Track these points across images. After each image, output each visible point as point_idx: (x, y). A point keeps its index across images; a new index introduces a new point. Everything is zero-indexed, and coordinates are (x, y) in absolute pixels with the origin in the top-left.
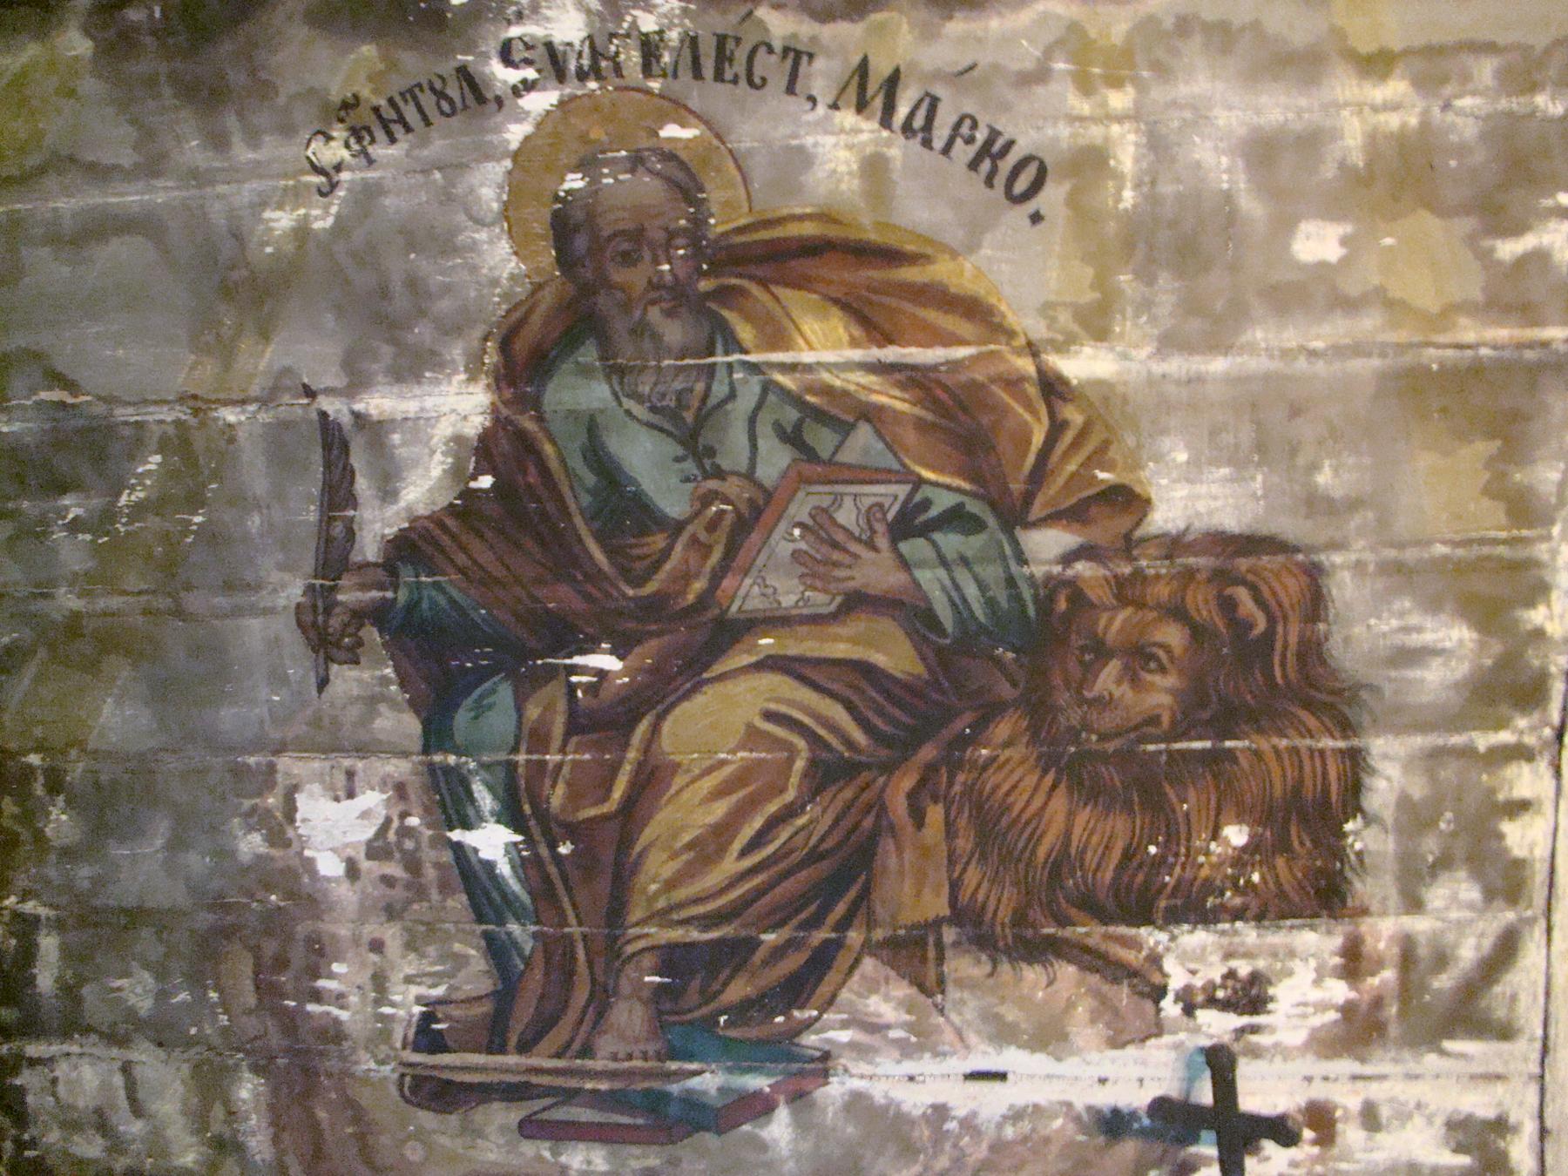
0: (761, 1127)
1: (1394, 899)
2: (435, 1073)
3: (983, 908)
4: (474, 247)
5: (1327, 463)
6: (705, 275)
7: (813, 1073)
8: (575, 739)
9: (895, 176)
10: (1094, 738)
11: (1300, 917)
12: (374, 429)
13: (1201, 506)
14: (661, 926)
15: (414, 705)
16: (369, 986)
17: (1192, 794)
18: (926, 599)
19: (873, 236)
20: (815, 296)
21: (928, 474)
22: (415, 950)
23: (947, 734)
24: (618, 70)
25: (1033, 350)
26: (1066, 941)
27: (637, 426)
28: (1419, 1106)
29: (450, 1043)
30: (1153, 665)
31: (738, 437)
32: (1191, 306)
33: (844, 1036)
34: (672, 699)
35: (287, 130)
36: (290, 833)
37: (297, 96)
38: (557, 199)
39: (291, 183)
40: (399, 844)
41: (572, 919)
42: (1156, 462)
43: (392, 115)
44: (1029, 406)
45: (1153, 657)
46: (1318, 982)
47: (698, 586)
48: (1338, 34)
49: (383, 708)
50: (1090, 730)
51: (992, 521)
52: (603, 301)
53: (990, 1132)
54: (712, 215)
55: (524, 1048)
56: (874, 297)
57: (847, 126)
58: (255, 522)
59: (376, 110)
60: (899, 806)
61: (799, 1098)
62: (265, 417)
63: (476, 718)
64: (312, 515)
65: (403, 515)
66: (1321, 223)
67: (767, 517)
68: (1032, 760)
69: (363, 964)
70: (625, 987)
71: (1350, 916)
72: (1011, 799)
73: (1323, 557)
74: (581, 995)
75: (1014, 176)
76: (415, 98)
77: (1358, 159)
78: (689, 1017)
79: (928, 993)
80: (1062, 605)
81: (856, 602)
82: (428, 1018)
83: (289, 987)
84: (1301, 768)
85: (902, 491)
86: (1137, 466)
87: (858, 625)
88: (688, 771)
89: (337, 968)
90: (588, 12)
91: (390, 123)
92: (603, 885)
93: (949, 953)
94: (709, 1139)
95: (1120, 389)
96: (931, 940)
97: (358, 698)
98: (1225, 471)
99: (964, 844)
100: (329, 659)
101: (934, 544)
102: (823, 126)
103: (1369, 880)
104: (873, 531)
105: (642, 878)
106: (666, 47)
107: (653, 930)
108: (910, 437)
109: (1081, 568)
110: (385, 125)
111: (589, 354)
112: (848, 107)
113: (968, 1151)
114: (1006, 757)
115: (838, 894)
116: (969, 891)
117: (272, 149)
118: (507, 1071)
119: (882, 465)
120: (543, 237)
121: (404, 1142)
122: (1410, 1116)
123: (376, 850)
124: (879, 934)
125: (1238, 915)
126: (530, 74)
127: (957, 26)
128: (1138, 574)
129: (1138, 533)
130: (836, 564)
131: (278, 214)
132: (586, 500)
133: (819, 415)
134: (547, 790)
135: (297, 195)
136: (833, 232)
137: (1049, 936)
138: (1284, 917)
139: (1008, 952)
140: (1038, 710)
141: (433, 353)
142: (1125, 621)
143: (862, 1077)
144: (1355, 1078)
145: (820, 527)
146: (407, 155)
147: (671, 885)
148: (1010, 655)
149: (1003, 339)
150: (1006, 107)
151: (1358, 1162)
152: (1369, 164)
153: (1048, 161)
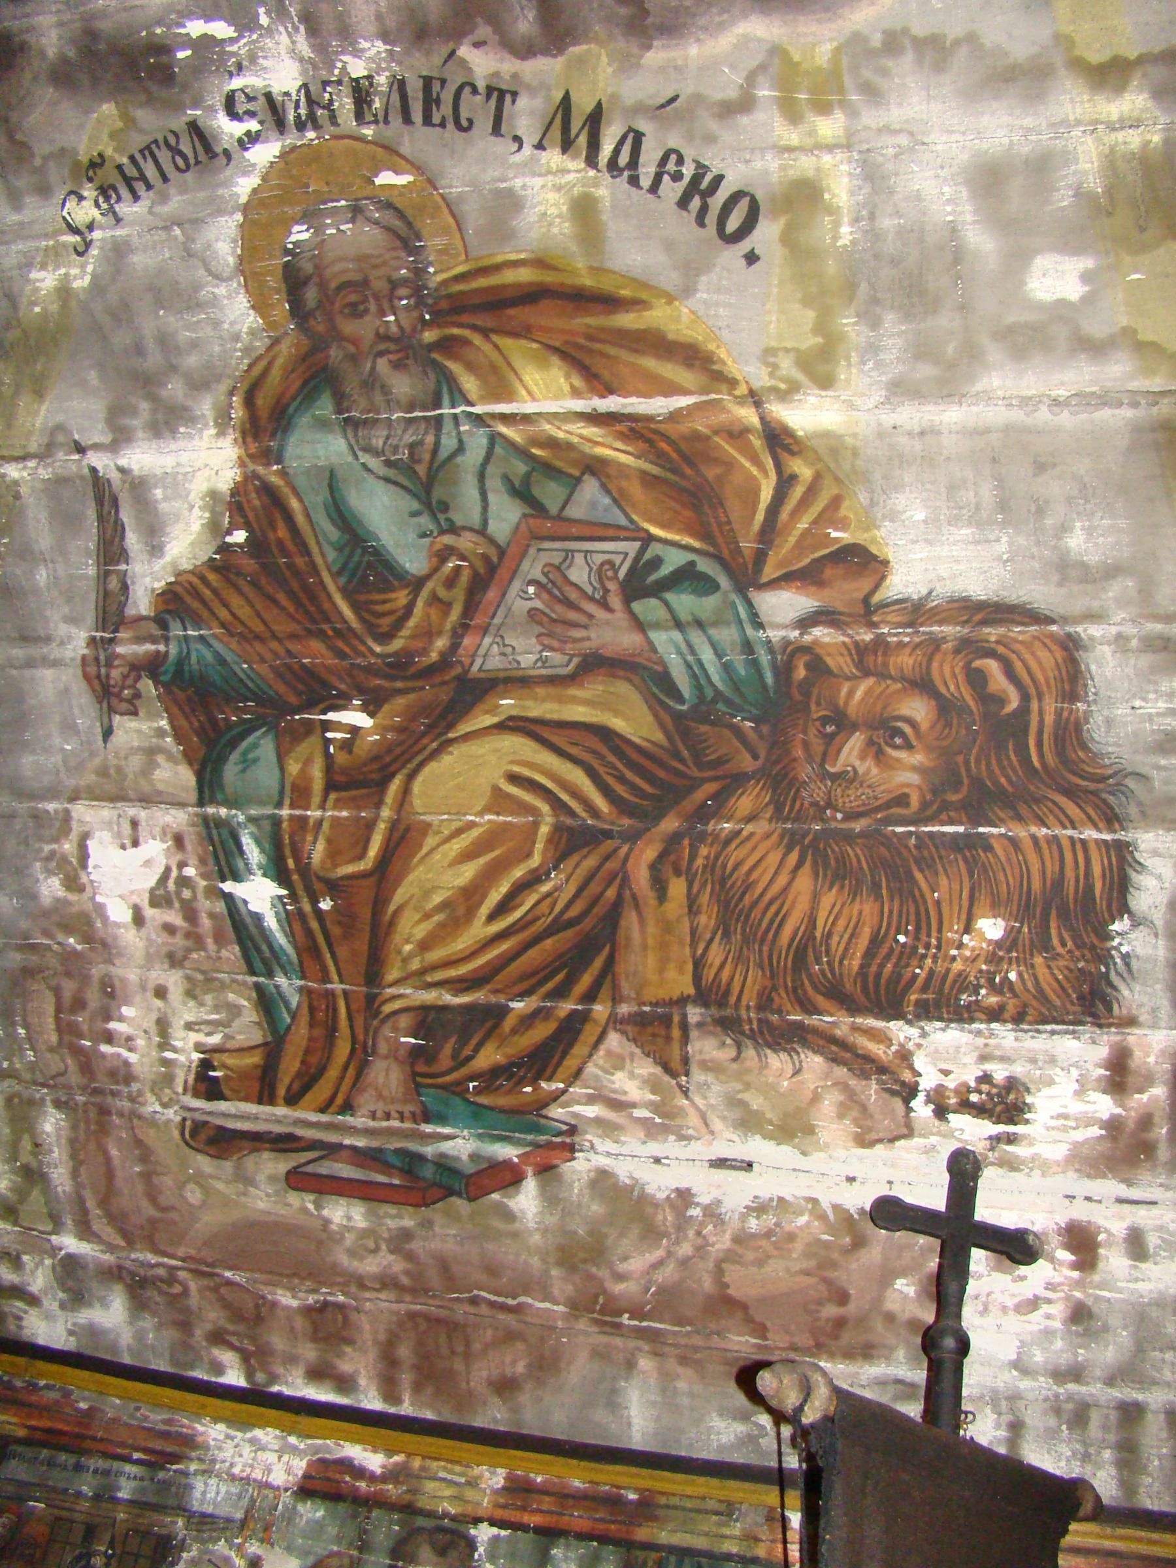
3: (727, 992)
4: (214, 301)
7: (563, 1146)
8: (333, 796)
9: (604, 218)
10: (839, 816)
11: (1064, 1023)
12: (139, 486)
13: (943, 570)
14: (416, 988)
16: (153, 1029)
17: (943, 881)
19: (588, 282)
20: (535, 346)
21: (655, 531)
22: (194, 997)
25: (755, 398)
26: (815, 1031)
27: (371, 479)
29: (227, 1092)
32: (922, 351)
33: (591, 1111)
34: (420, 758)
35: (44, 191)
36: (84, 879)
37: (51, 156)
38: (287, 252)
40: (178, 893)
41: (336, 977)
44: (755, 460)
45: (898, 732)
46: (1080, 1093)
47: (441, 643)
48: (1064, 41)
50: (836, 809)
51: (724, 581)
52: (335, 354)
53: (734, 1224)
54: (430, 264)
55: (292, 1100)
59: (119, 167)
60: (641, 877)
61: (546, 1170)
62: (45, 473)
63: (244, 771)
66: (1059, 258)
67: (503, 573)
68: (775, 837)
69: (149, 1009)
70: (383, 1048)
71: (1118, 1026)
73: (1079, 629)
74: (343, 1049)
75: (728, 216)
77: (1095, 185)
78: (440, 1080)
79: (673, 1074)
80: (801, 673)
81: (594, 664)
82: (206, 1065)
83: (85, 1028)
85: (632, 547)
87: (594, 688)
88: (438, 832)
89: (126, 1011)
90: (302, 60)
91: (134, 183)
93: (694, 1034)
95: (849, 440)
96: (676, 1019)
97: (139, 749)
100: (111, 710)
101: (667, 604)
102: (530, 168)
104: (606, 591)
105: (397, 938)
106: (377, 93)
107: (409, 991)
108: (636, 490)
109: (819, 633)
110: (128, 181)
111: (324, 407)
112: (553, 146)
115: (587, 963)
116: (713, 971)
117: (36, 211)
123: (158, 898)
124: (624, 1009)
125: (995, 1015)
126: (253, 125)
127: (656, 56)
128: (880, 641)
129: (877, 598)
131: (42, 274)
132: (331, 555)
133: (549, 470)
135: (57, 254)
136: (548, 278)
137: (795, 1022)
138: (1045, 1022)
139: (752, 1036)
140: (780, 781)
141: (186, 409)
143: (608, 1154)
144: (1121, 1201)
145: (554, 586)
146: (150, 212)
147: (424, 946)
149: (724, 387)
152: (1110, 191)
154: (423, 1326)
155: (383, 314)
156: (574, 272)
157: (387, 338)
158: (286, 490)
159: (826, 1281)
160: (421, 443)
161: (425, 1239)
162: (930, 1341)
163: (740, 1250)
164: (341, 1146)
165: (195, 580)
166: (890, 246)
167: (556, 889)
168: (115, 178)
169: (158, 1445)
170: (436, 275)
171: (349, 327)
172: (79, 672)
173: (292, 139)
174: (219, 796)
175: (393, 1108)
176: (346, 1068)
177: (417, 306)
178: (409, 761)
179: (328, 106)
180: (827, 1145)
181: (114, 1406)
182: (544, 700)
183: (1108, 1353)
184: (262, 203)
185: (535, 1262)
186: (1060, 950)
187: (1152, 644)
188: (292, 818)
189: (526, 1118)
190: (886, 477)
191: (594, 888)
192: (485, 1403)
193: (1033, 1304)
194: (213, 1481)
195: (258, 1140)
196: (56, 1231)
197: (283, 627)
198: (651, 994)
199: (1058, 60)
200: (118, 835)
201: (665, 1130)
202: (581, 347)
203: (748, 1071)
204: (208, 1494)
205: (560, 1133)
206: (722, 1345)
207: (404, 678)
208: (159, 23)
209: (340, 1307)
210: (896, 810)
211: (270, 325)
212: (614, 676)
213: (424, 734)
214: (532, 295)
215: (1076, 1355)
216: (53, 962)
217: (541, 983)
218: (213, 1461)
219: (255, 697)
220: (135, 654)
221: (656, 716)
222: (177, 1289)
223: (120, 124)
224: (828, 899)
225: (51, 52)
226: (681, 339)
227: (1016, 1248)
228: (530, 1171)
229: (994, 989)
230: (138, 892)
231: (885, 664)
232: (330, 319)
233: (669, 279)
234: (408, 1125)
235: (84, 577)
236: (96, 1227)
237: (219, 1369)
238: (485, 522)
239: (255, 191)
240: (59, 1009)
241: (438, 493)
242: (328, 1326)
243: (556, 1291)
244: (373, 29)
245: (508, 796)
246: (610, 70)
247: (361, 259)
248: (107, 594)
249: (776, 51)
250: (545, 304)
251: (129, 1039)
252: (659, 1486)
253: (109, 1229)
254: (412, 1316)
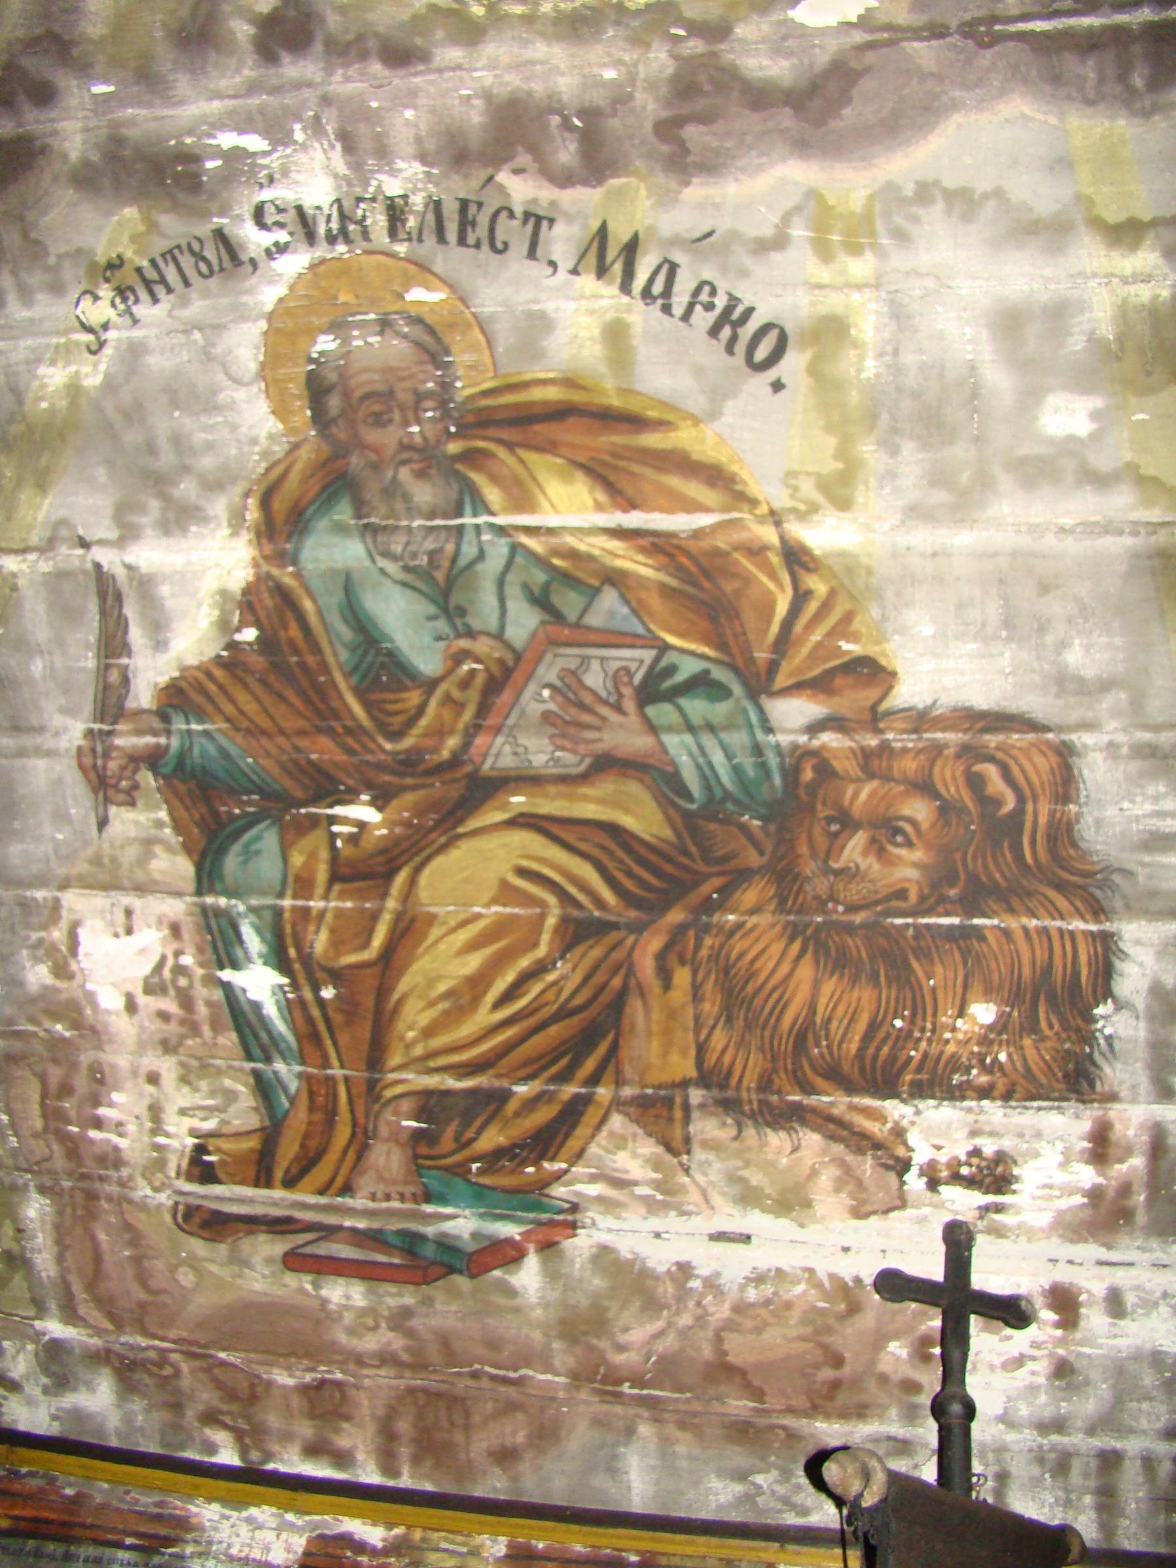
0: (511, 1273)
1: (1143, 1080)
2: (204, 1203)
3: (729, 1073)
4: (232, 406)
5: (1077, 641)
6: (450, 436)
8: (337, 888)
9: (635, 342)
10: (840, 908)
11: (1048, 1099)
12: (145, 584)
13: (948, 681)
14: (419, 1073)
15: (187, 848)
16: (145, 1115)
17: (939, 970)
18: (673, 763)
19: (616, 402)
20: (559, 461)
21: (672, 640)
23: (694, 897)
24: (365, 234)
25: (775, 518)
26: (813, 1110)
27: (388, 585)
28: (1165, 1295)
29: (221, 1175)
30: (899, 839)
31: (488, 600)
32: (938, 478)
33: (593, 1190)
35: (57, 289)
36: (74, 966)
38: (311, 361)
39: (63, 340)
40: (174, 981)
41: (336, 1063)
42: (902, 634)
43: (154, 276)
44: (773, 575)
45: (898, 831)
46: (1064, 1165)
47: (452, 742)
48: (1084, 202)
49: (158, 849)
50: (837, 902)
51: (737, 689)
52: (356, 462)
54: (457, 378)
55: (290, 1183)
56: (622, 464)
57: (588, 292)
58: (37, 667)
59: (139, 270)
60: (646, 966)
61: (548, 1247)
62: (45, 566)
64: (90, 662)
65: (174, 664)
66: (1070, 397)
67: (518, 676)
68: (778, 928)
69: (141, 1095)
70: (384, 1131)
71: (1100, 1101)
72: (757, 965)
73: (1074, 737)
74: (343, 1133)
75: (757, 346)
76: (175, 259)
77: (1107, 332)
79: (674, 1153)
80: (808, 775)
81: (606, 764)
82: (200, 1149)
83: (73, 1114)
84: (1051, 949)
85: (648, 655)
86: (881, 638)
87: (606, 786)
89: (116, 1096)
90: (336, 176)
91: (153, 285)
92: (365, 1031)
93: (695, 1114)
94: (461, 1281)
95: (864, 560)
96: (678, 1100)
97: (136, 839)
98: (972, 646)
99: (710, 1007)
100: (107, 800)
101: (680, 709)
103: (1119, 1066)
104: (620, 695)
105: (400, 1026)
106: (412, 212)
107: (411, 1076)
108: (655, 601)
109: (828, 738)
110: (148, 284)
111: (343, 512)
113: (712, 1309)
114: (752, 923)
117: (45, 308)
118: (275, 1204)
119: (626, 628)
120: (300, 398)
121: (176, 1267)
122: (1156, 1305)
123: (150, 988)
124: (627, 1092)
125: (985, 1093)
126: (282, 236)
127: (696, 191)
128: (885, 747)
129: (884, 706)
130: (588, 727)
131: (51, 370)
132: (344, 655)
133: (567, 579)
134: (310, 937)
136: (577, 397)
138: (1032, 1098)
139: (752, 1116)
140: (785, 878)
141: (198, 508)
142: (871, 795)
143: (610, 1230)
144: (1101, 1263)
145: (570, 690)
147: (429, 1032)
148: (756, 823)
149: (746, 507)
150: (744, 273)
151: (1100, 1347)
152: (1120, 338)
153: (789, 329)
154: (422, 1399)
155: (407, 424)
156: (602, 392)
157: (411, 447)
158: (300, 592)
159: (824, 1347)
160: (441, 550)
161: (427, 1316)
162: (938, 1409)
163: (739, 1319)
164: (339, 1228)
165: (200, 676)
166: (911, 381)
167: (563, 978)
168: (133, 280)
170: (463, 389)
171: (372, 436)
172: (74, 763)
173: (322, 251)
174: (219, 886)
175: (393, 1190)
176: (345, 1151)
177: (441, 419)
178: (417, 854)
179: (361, 222)
180: (823, 1218)
181: (102, 1491)
182: (554, 798)
183: (1089, 1405)
184: (288, 312)
185: (537, 1335)
186: (1048, 1032)
187: (1148, 753)
188: (294, 909)
189: (531, 1197)
190: (899, 595)
191: (599, 978)
192: (485, 1473)
193: (1019, 1361)
195: (252, 1223)
196: (38, 1317)
197: (293, 724)
198: (655, 1077)
199: (1078, 217)
200: (112, 923)
201: (665, 1206)
202: (604, 464)
203: (749, 1149)
205: (561, 1211)
206: (722, 1409)
207: (413, 775)
208: (190, 133)
209: (338, 1384)
210: (895, 904)
211: (291, 431)
212: (625, 776)
213: (431, 830)
214: (560, 413)
215: (1058, 1408)
216: (39, 1048)
217: (544, 1068)
218: (210, 1543)
219: (260, 791)
220: (134, 747)
221: (666, 814)
222: (168, 1371)
223: (142, 228)
224: (829, 987)
225: (74, 156)
226: (705, 459)
227: (1010, 1312)
228: (531, 1247)
229: (986, 1069)
231: (890, 768)
232: (353, 424)
233: (696, 403)
234: (408, 1206)
236: (82, 1311)
237: (212, 1449)
238: (502, 627)
239: (281, 300)
240: (44, 1095)
241: (456, 599)
242: (326, 1403)
243: (557, 1363)
244: (411, 150)
245: (516, 889)
246: (648, 203)
247: (389, 370)
248: (106, 687)
249: (813, 195)
250: (571, 421)
251: (120, 1124)
252: (660, 1547)
253: (96, 1313)
254: (411, 1391)
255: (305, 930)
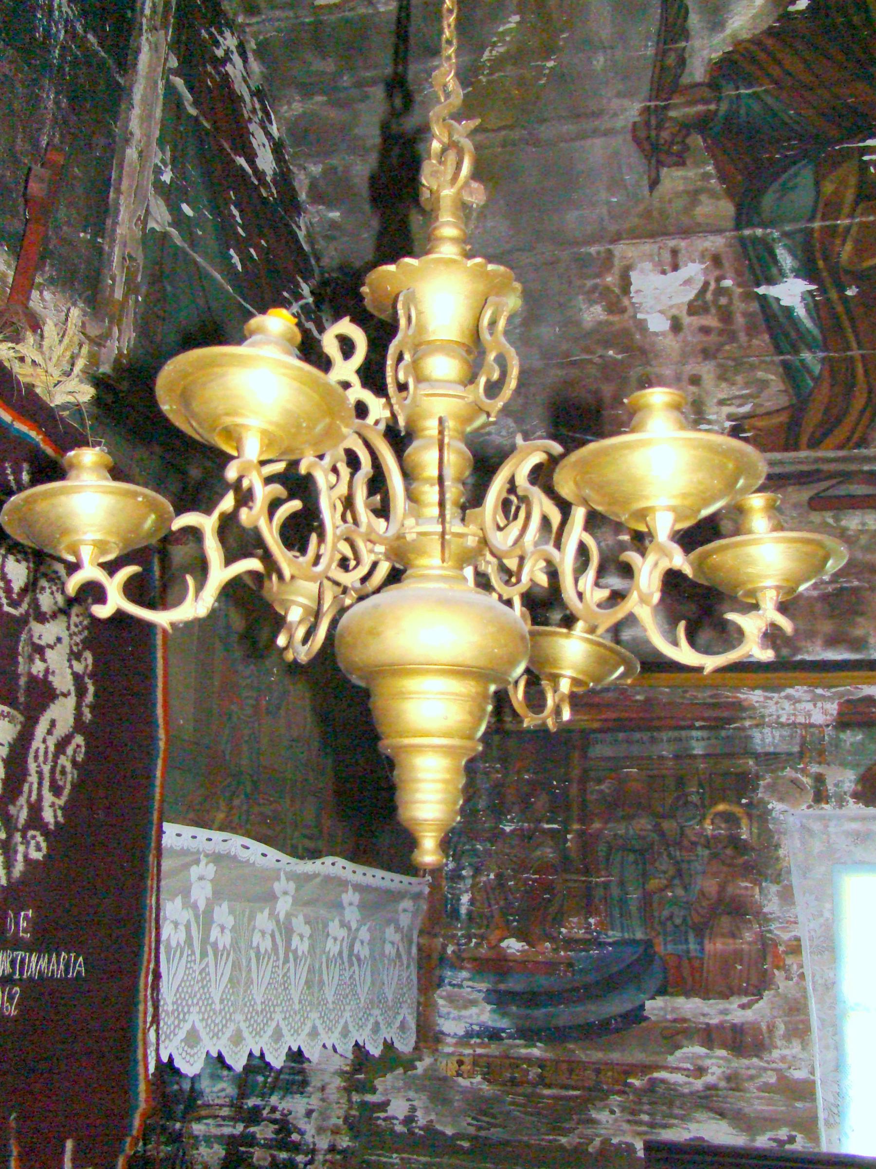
8: (862, 206)
15: (730, 194)
36: (626, 302)
40: (715, 302)
41: (854, 345)
49: (703, 198)
55: (814, 444)
58: (599, 62)
65: (729, 40)
97: (684, 191)
100: (660, 163)
123: (693, 309)
165: (753, 48)
169: (708, 713)
172: (629, 137)
174: (756, 219)
176: (863, 412)
194: (767, 730)
200: (660, 263)
204: (765, 739)
209: (854, 591)
218: (763, 717)
220: (687, 116)
230: (678, 306)
235: (645, 57)
248: (662, 69)
255: (832, 243)
